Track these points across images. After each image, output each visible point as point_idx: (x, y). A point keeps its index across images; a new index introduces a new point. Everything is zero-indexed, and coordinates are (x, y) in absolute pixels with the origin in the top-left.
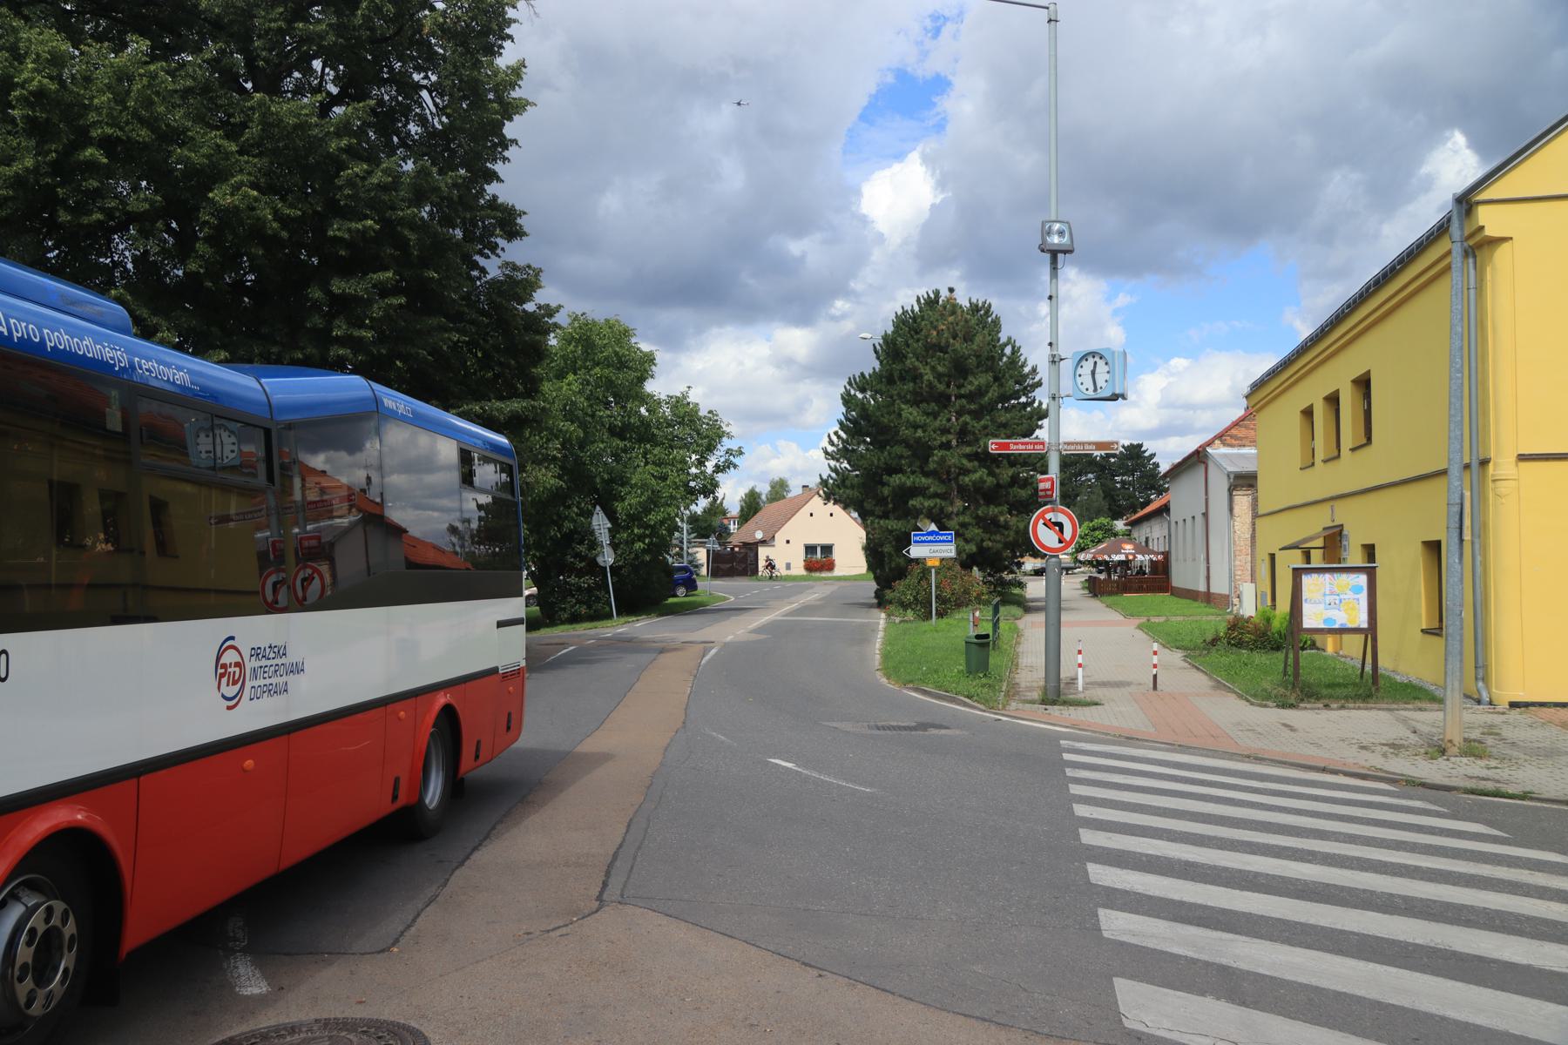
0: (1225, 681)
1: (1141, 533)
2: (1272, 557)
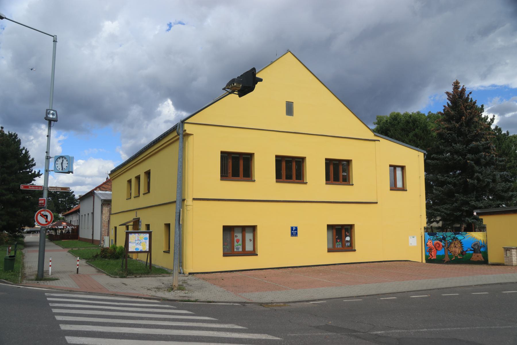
0: (102, 270)
1: (68, 219)
2: (116, 228)
